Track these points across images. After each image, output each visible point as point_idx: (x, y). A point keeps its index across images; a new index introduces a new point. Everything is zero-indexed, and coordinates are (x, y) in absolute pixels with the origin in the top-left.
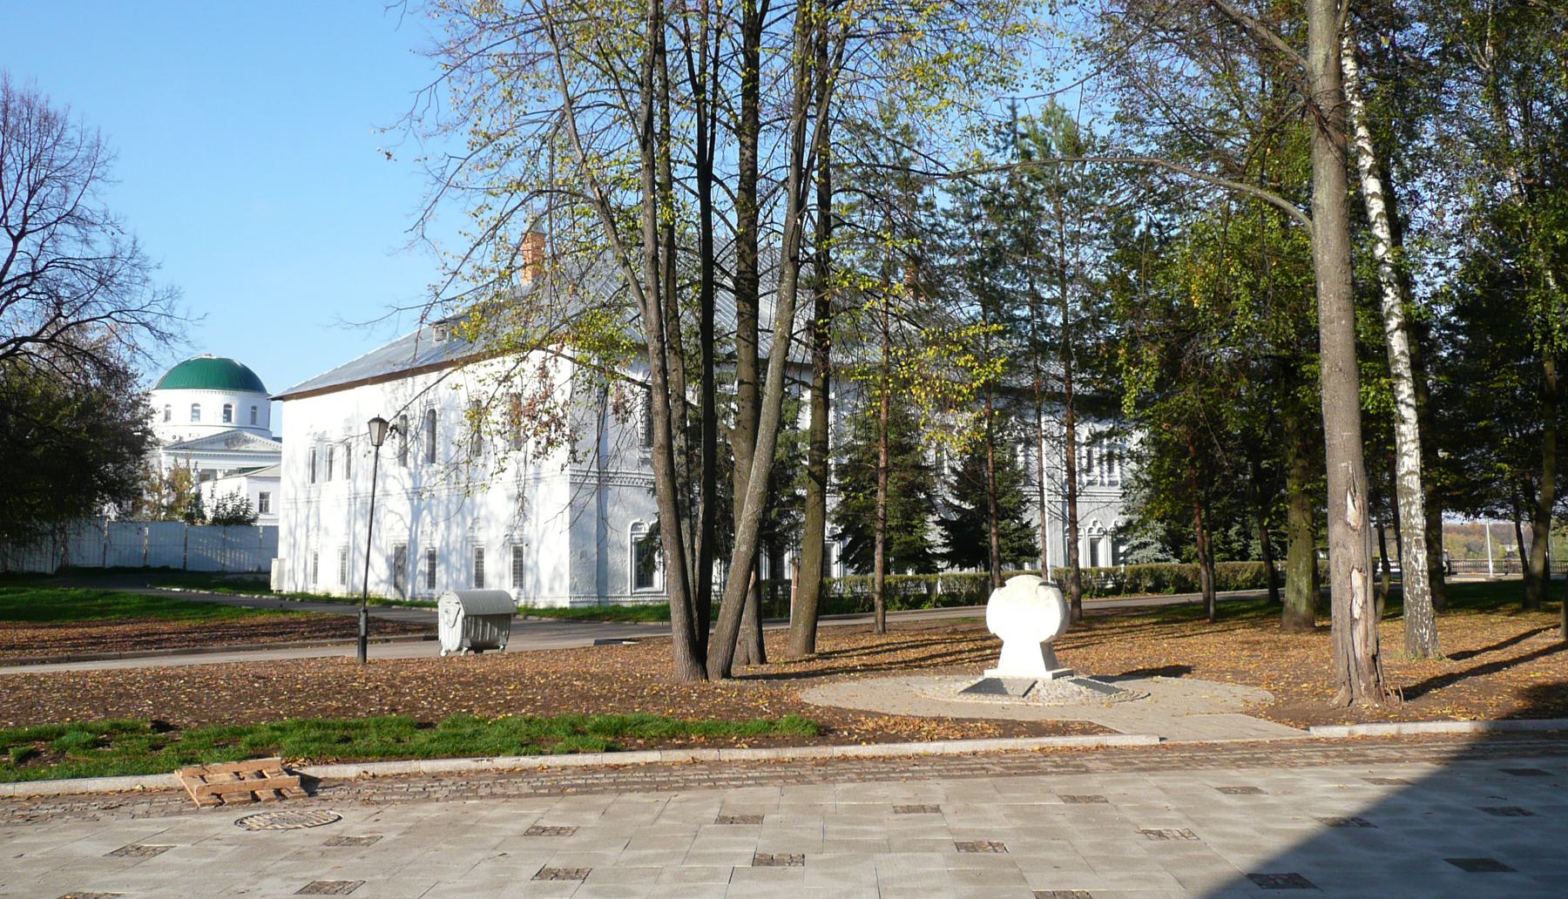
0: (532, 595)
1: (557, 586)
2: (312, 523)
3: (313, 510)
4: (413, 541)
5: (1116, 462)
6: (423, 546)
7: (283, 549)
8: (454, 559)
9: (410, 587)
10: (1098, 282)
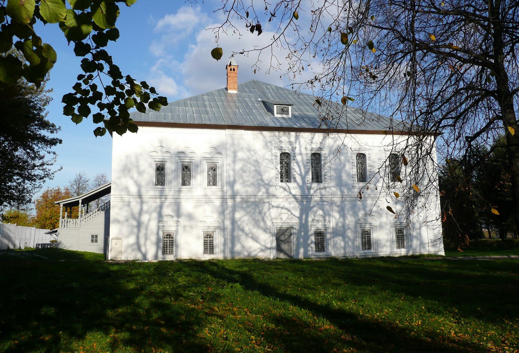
2: (167, 211)
4: (304, 226)
8: (349, 234)
9: (302, 251)
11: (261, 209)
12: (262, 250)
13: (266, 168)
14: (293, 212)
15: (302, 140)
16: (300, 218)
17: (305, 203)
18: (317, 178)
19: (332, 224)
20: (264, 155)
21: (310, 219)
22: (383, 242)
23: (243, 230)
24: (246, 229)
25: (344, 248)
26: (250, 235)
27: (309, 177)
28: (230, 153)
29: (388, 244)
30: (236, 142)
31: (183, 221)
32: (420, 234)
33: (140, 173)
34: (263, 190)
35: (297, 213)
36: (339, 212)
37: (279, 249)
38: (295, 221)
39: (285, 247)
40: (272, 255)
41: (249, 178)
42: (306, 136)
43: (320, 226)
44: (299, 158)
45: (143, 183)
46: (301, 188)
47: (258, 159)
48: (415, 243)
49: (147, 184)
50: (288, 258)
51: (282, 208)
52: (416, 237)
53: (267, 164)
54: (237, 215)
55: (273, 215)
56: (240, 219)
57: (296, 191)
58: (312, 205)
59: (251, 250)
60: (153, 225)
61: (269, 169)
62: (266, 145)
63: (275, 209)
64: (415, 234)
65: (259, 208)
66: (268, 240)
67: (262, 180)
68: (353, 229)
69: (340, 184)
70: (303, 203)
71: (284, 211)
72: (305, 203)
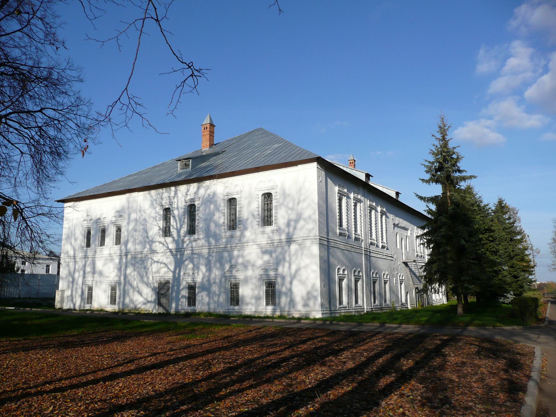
0: (287, 309)
1: (311, 303)
2: (88, 269)
3: (89, 261)
4: (177, 279)
5: (36, 256)
6: (186, 280)
7: (62, 285)
8: (215, 288)
9: (174, 305)
10: (213, 238)
11: (146, 264)
12: (145, 304)
13: (151, 226)
14: (170, 267)
15: (180, 194)
16: (174, 272)
17: (179, 256)
18: (192, 231)
19: (199, 279)
20: (150, 213)
21: (182, 273)
22: (248, 300)
23: (131, 285)
24: (135, 284)
25: (209, 304)
26: (137, 289)
27: (185, 229)
28: (126, 216)
29: (253, 301)
30: (131, 206)
31: (96, 275)
32: (290, 290)
33: (76, 240)
34: (148, 246)
35: (172, 268)
36: (206, 266)
37: (113, 300)
38: (170, 276)
39: (163, 301)
40: (151, 308)
41: (138, 236)
42: (183, 188)
43: (189, 280)
44: (176, 212)
45: (77, 248)
46: (176, 242)
47: (146, 217)
48: (284, 300)
49: (79, 248)
50: (165, 312)
51: (161, 263)
52: (286, 294)
53: (152, 221)
54: (129, 271)
55: (154, 270)
56: (130, 275)
57: (172, 246)
58: (184, 259)
59: (137, 303)
60: (80, 281)
61: (153, 226)
62: (152, 203)
63: (156, 263)
64: (284, 289)
65: (144, 264)
66: (148, 294)
67: (147, 237)
68: (219, 283)
69: (208, 234)
70: (177, 257)
71: (162, 265)
72: (179, 256)
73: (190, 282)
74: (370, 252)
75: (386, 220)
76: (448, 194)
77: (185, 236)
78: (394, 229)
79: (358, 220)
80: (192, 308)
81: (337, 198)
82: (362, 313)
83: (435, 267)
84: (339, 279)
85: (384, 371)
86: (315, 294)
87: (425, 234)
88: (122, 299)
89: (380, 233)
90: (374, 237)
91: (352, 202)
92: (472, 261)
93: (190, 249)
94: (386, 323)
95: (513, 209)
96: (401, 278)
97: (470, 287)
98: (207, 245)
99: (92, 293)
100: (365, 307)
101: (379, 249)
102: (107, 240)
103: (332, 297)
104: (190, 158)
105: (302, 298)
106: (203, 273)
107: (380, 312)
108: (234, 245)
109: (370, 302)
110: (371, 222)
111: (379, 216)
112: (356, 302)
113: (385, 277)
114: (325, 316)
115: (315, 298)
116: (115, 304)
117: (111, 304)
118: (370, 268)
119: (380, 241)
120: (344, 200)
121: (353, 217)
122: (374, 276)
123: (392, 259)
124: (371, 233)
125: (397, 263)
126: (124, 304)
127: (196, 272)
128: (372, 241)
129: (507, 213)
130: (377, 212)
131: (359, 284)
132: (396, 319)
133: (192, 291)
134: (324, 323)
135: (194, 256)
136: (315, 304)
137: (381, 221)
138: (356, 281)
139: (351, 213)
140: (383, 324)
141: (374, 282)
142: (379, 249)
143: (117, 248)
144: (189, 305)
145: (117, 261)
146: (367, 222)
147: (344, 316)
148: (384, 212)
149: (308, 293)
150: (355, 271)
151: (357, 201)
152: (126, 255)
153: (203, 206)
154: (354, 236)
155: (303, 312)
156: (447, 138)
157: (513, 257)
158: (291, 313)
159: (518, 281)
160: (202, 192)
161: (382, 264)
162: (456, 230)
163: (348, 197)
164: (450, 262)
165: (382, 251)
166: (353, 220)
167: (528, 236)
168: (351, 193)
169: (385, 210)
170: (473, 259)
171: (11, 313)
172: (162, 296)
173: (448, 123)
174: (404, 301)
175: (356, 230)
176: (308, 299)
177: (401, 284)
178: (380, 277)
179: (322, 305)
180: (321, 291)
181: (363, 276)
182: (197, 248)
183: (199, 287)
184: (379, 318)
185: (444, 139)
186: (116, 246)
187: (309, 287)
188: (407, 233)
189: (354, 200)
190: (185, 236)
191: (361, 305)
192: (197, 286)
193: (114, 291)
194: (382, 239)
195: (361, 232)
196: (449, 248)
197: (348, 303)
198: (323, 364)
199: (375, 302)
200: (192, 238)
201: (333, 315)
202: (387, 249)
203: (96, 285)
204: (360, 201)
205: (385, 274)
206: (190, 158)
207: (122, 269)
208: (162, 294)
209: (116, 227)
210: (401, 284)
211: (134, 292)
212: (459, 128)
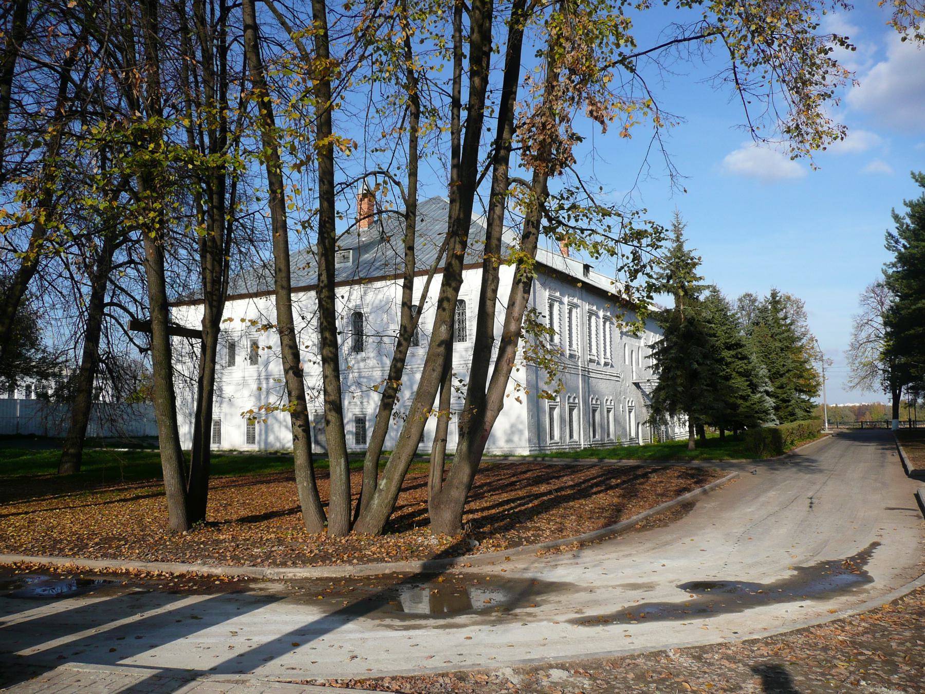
1: (516, 438)
26: (284, 423)
37: (251, 438)
43: (357, 411)
73: (357, 413)
74: (589, 372)
75: (610, 327)
76: (682, 307)
77: (349, 354)
78: (621, 339)
79: (574, 331)
80: (362, 446)
81: (547, 305)
82: (578, 450)
83: (663, 394)
84: (550, 408)
85: (597, 485)
86: (521, 427)
87: (655, 354)
88: (263, 437)
89: (602, 345)
90: (594, 351)
91: (566, 308)
92: (705, 387)
93: (357, 371)
94: (605, 458)
95: (797, 302)
96: (630, 405)
97: (701, 417)
98: (380, 366)
99: (220, 430)
100: (582, 443)
101: (601, 368)
102: (239, 359)
103: (541, 430)
104: (351, 249)
105: (505, 432)
106: (374, 402)
107: (601, 448)
108: (416, 366)
109: (588, 436)
110: (590, 333)
111: (602, 324)
112: (571, 436)
113: (608, 403)
114: (533, 453)
115: (521, 432)
116: (253, 442)
117: (247, 443)
118: (589, 392)
119: (603, 356)
120: (556, 305)
121: (567, 328)
122: (594, 402)
123: (618, 379)
124: (590, 347)
125: (625, 384)
126: (266, 443)
127: (365, 400)
128: (592, 357)
129: (782, 310)
130: (599, 318)
131: (575, 412)
132: (618, 455)
133: (361, 425)
134: (536, 460)
135: (362, 380)
136: (520, 440)
137: (604, 329)
138: (571, 410)
139: (565, 323)
140: (601, 460)
141: (594, 411)
142: (601, 368)
143: (252, 371)
144: (358, 442)
145: (254, 386)
146: (585, 332)
147: (556, 453)
148: (608, 317)
149: (513, 426)
150: (569, 397)
151: (573, 306)
152: (267, 379)
153: (373, 315)
154: (568, 352)
155: (506, 449)
156: (683, 239)
157: (784, 374)
158: (490, 450)
159: (787, 407)
160: (370, 297)
161: (604, 387)
162: (689, 351)
163: (561, 303)
164: (680, 389)
165: (605, 369)
166: (567, 332)
167: (817, 341)
168: (564, 297)
169: (608, 314)
170: (707, 385)
171: (149, 452)
172: (319, 432)
173: (684, 221)
174: (633, 435)
175: (570, 345)
176: (513, 433)
177: (630, 412)
178: (601, 404)
179: (530, 441)
180: (529, 423)
181: (579, 403)
182: (366, 370)
183: (370, 420)
184: (598, 455)
185: (678, 240)
186: (252, 366)
187: (513, 420)
188: (639, 343)
189: (568, 305)
190: (349, 354)
191: (577, 440)
192: (367, 418)
193: (251, 427)
194: (605, 354)
195: (578, 347)
196: (679, 373)
197: (561, 438)
198: (548, 484)
199: (594, 436)
200: (359, 357)
201: (543, 452)
202: (612, 366)
203: (225, 418)
204: (576, 306)
205: (608, 399)
206: (351, 249)
207: (263, 397)
208: (319, 429)
209: (251, 340)
210: (630, 412)
211: (280, 427)
212: (733, 153)
